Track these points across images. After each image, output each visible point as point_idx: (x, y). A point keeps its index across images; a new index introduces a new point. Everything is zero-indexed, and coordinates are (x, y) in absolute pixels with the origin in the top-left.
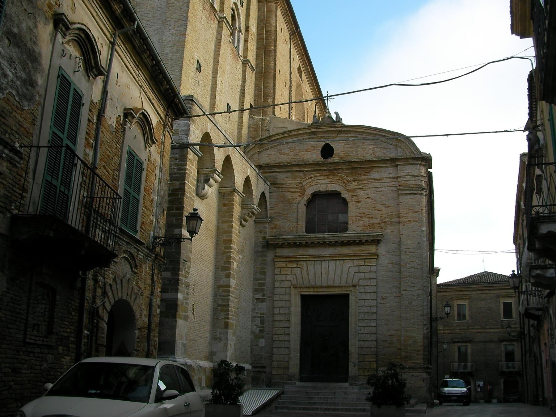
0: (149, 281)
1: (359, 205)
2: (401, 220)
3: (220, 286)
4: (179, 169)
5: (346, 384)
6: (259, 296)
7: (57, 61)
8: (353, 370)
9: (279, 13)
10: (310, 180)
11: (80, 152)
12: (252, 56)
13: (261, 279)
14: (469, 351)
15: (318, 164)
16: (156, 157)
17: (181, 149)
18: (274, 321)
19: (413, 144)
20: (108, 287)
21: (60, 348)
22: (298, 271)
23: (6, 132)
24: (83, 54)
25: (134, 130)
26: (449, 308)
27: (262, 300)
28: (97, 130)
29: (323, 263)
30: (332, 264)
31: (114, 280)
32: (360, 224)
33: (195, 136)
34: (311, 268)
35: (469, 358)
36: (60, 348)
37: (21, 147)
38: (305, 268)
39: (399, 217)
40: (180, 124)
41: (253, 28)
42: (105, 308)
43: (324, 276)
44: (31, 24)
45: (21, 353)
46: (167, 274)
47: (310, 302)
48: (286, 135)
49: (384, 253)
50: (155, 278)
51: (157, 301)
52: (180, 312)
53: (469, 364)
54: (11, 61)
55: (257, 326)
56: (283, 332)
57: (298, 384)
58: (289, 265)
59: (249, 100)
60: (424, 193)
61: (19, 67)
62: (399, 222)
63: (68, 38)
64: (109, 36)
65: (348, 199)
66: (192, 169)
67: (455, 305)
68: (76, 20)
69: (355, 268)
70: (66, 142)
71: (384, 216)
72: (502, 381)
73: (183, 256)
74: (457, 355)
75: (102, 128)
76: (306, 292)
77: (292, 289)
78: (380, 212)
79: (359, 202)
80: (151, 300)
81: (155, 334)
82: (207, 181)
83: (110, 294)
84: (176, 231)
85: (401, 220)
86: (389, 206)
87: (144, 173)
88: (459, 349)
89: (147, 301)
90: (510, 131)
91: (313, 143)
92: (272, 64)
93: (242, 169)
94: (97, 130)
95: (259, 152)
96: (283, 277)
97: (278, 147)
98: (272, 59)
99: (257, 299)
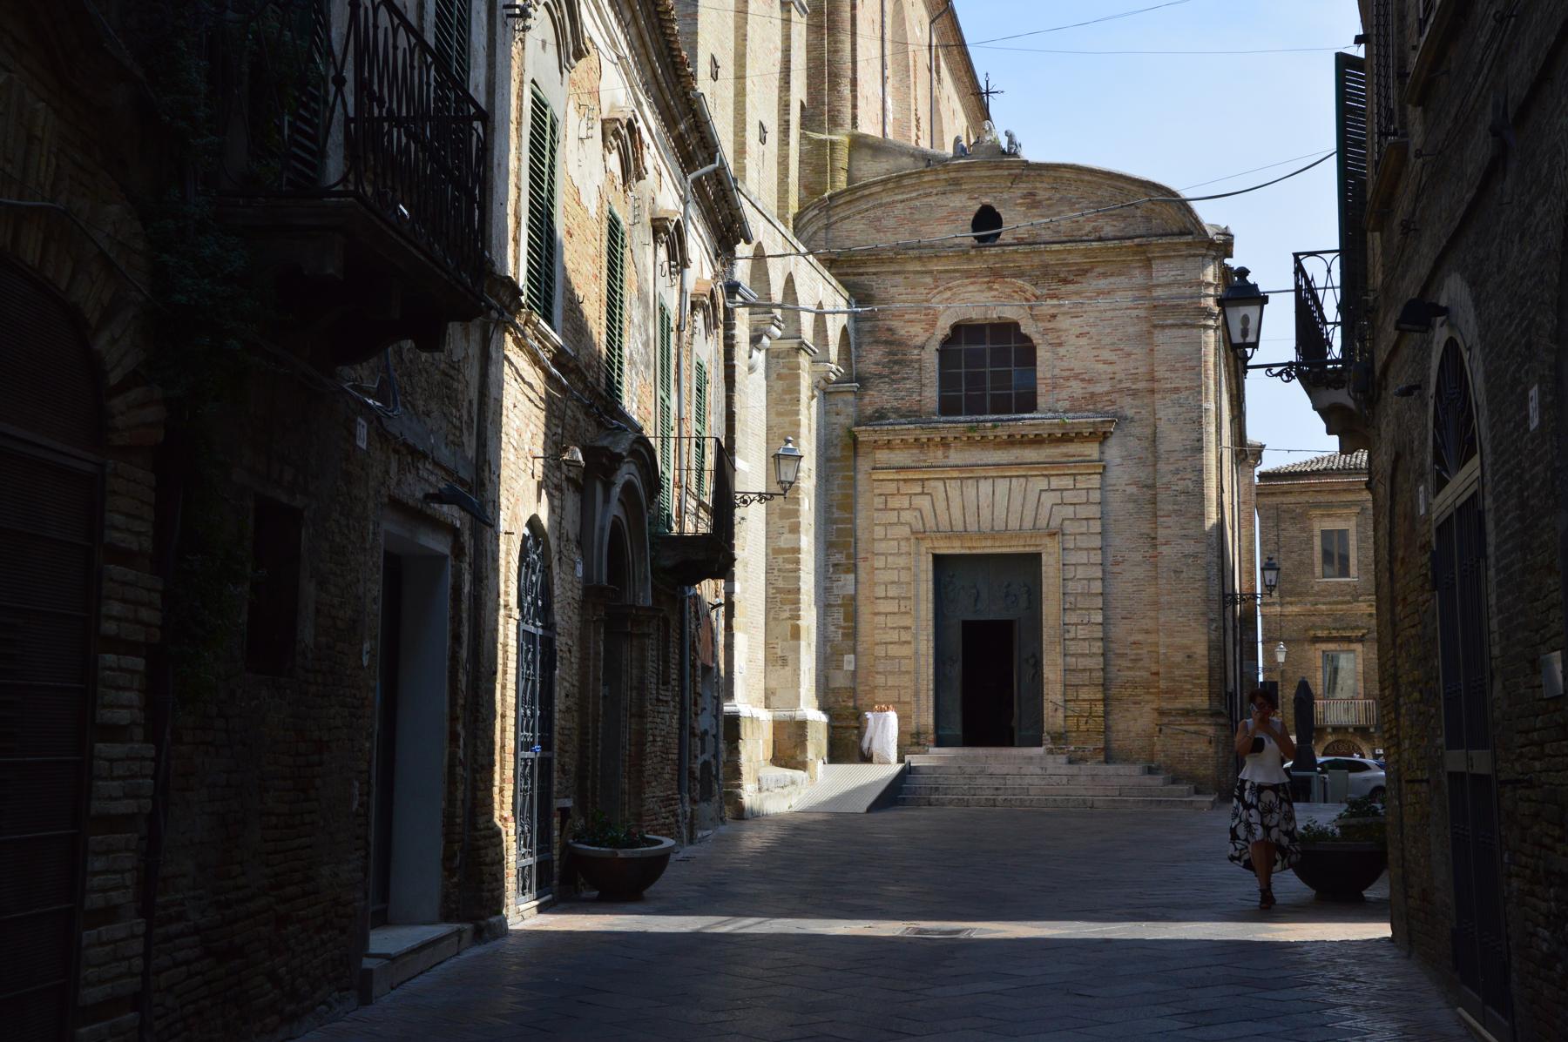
1: (1062, 351)
2: (1156, 385)
5: (1040, 750)
6: (839, 558)
8: (1053, 718)
10: (948, 294)
13: (843, 521)
15: (963, 253)
18: (876, 614)
19: (1190, 211)
22: (924, 503)
26: (1274, 573)
29: (982, 483)
30: (1002, 485)
32: (1064, 394)
34: (954, 493)
38: (941, 495)
39: (1153, 380)
48: (891, 185)
49: (1118, 461)
55: (839, 627)
56: (895, 638)
58: (905, 489)
60: (1211, 322)
62: (1152, 391)
65: (1036, 339)
67: (1317, 532)
69: (1052, 494)
71: (1118, 377)
76: (945, 548)
78: (1109, 368)
79: (1060, 345)
85: (1156, 385)
86: (1129, 355)
91: (957, 201)
95: (828, 227)
96: (893, 517)
97: (871, 214)
99: (835, 565)
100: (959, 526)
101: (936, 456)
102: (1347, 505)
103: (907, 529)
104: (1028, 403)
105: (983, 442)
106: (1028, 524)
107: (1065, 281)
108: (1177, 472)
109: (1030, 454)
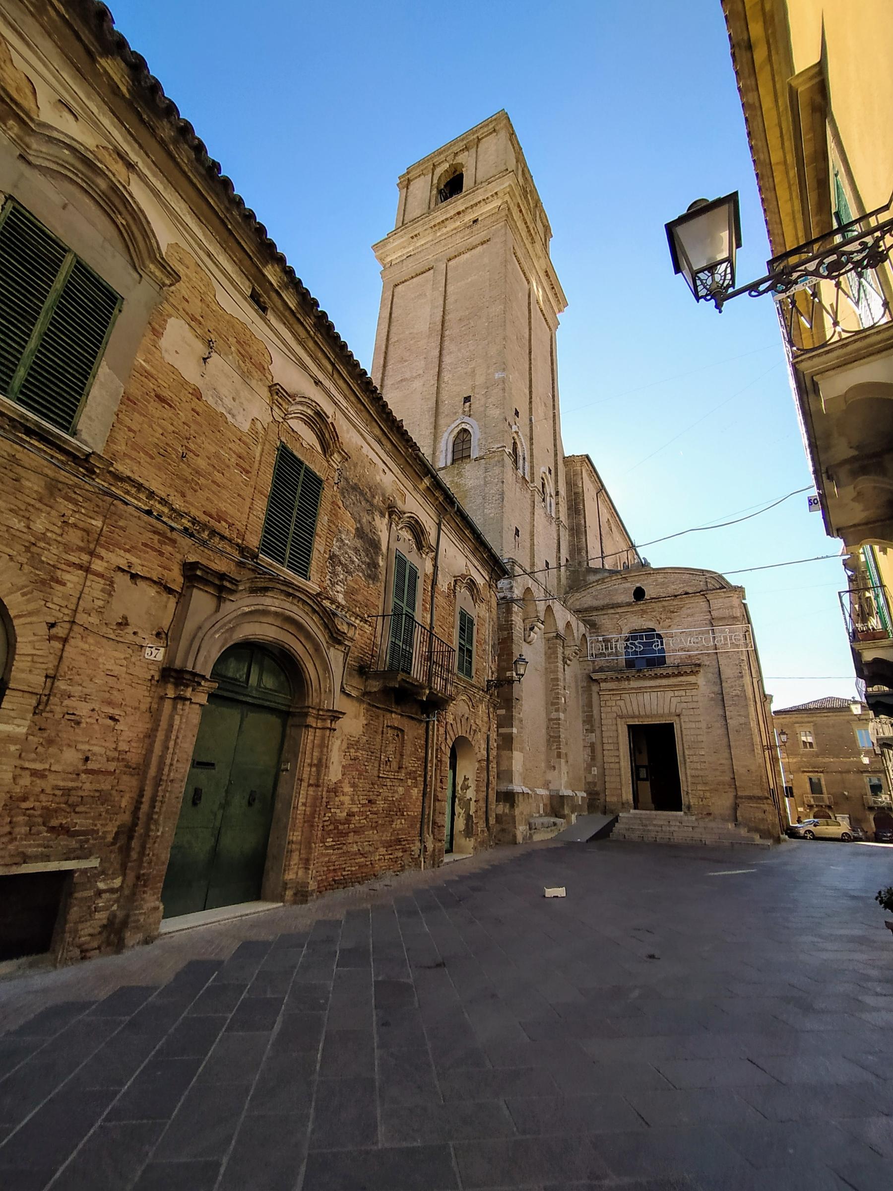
0: (486, 719)
3: (550, 720)
4: (507, 621)
5: (682, 813)
7: (394, 546)
9: (585, 475)
11: (418, 617)
12: (563, 517)
14: (823, 783)
15: (629, 604)
16: (484, 615)
17: (506, 604)
19: (724, 579)
20: (449, 727)
21: (409, 781)
22: (621, 703)
23: (356, 606)
24: (415, 537)
25: (463, 592)
27: (592, 731)
28: (432, 597)
31: (454, 719)
33: (518, 593)
35: (824, 790)
36: (409, 781)
37: (369, 616)
40: (503, 583)
41: (563, 491)
42: (446, 743)
43: (648, 707)
44: (370, 518)
45: (376, 786)
46: (502, 712)
47: (636, 732)
50: (491, 716)
51: (494, 736)
52: (515, 744)
53: (825, 796)
54: (356, 550)
57: (632, 811)
59: (564, 554)
61: (363, 554)
63: (400, 526)
64: (435, 519)
66: (517, 619)
68: (406, 510)
70: (406, 609)
72: (872, 817)
73: (515, 696)
74: (808, 785)
75: (436, 595)
77: (619, 720)
80: (488, 736)
81: (493, 765)
82: (532, 629)
83: (451, 733)
84: (508, 674)
87: (475, 628)
88: (810, 779)
89: (485, 737)
90: (822, 558)
92: (153, 241)
93: (562, 616)
94: (432, 597)
96: (609, 709)
98: (582, 517)
100: (637, 713)
101: (625, 684)
102: (809, 722)
103: (126, 561)
104: (665, 663)
105: (645, 678)
106: (666, 711)
107: (673, 612)
108: (732, 687)
109: (664, 682)
